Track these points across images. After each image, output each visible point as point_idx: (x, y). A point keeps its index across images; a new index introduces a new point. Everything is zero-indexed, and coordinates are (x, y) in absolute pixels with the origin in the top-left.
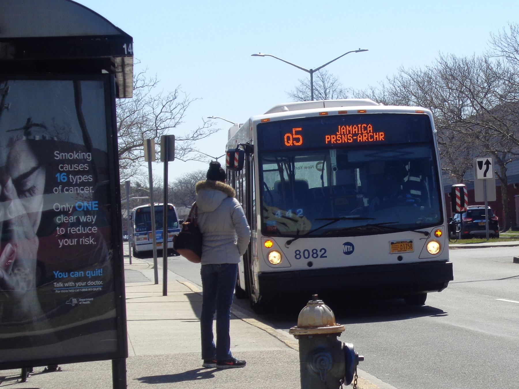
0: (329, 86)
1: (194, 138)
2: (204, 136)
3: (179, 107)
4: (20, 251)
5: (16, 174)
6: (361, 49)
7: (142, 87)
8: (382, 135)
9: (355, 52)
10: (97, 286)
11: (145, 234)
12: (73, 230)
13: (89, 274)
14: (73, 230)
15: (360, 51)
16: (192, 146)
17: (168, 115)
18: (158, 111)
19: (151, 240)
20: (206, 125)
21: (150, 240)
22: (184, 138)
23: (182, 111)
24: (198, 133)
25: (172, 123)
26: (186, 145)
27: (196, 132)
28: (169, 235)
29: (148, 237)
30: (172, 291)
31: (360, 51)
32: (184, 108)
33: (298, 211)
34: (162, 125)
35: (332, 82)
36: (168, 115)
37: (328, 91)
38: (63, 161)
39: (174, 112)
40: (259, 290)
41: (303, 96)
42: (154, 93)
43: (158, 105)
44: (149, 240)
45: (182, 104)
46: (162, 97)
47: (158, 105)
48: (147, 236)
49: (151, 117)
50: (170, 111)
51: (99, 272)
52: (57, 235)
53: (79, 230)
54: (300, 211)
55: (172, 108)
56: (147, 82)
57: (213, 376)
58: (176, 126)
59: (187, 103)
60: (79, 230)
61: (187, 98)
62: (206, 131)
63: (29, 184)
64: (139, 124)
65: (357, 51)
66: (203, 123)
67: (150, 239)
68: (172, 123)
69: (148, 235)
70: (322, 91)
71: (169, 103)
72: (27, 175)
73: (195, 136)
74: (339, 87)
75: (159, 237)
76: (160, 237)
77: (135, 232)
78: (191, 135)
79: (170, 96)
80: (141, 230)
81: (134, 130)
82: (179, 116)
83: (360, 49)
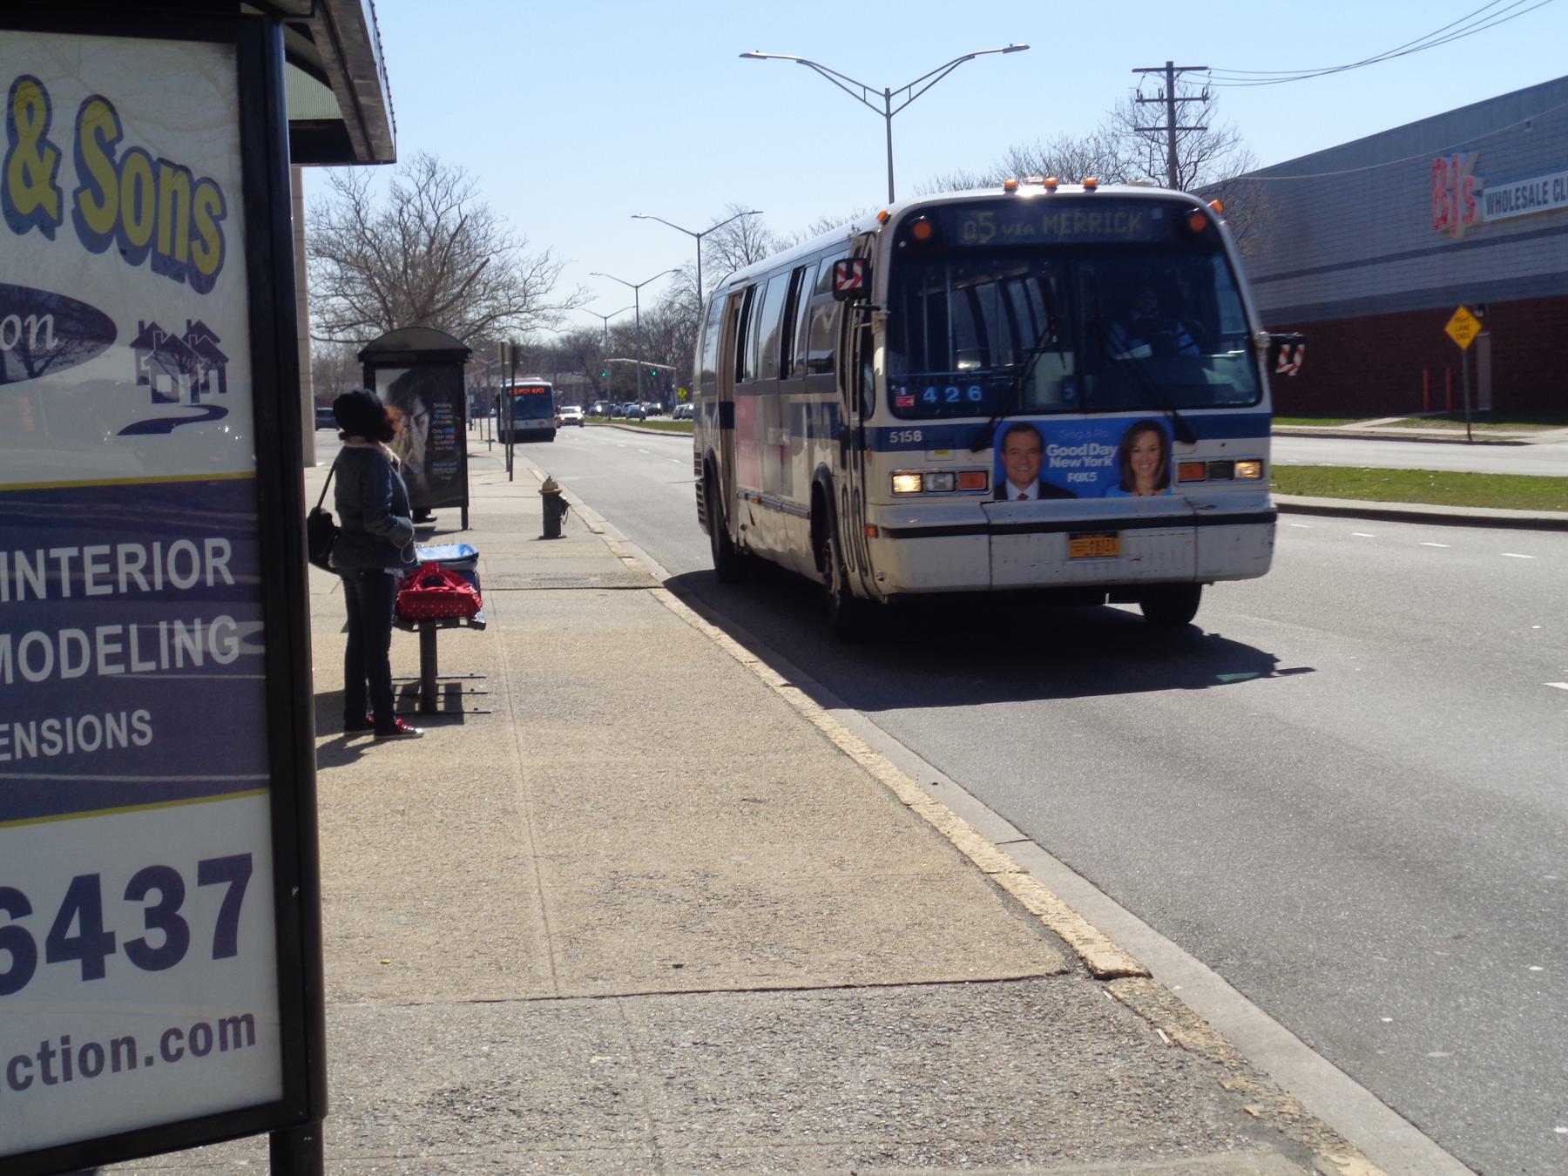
1: (567, 307)
3: (551, 271)
4: (416, 453)
5: (415, 415)
8: (218, 552)
10: (453, 470)
11: (976, 440)
12: (442, 443)
13: (451, 464)
14: (442, 443)
16: (567, 316)
17: (539, 280)
18: (526, 275)
19: (1023, 497)
21: (1013, 491)
22: (556, 306)
25: (543, 288)
29: (1000, 465)
30: (637, 592)
32: (557, 270)
34: (532, 291)
36: (539, 280)
38: (438, 408)
39: (545, 276)
42: (523, 254)
43: (527, 267)
44: (1001, 494)
47: (527, 267)
48: (986, 458)
49: (520, 280)
51: (455, 463)
52: (1000, 280)
53: (446, 442)
59: (560, 266)
60: (446, 442)
62: (581, 298)
63: (421, 420)
64: (507, 286)
67: (1015, 482)
68: (543, 288)
69: (1002, 449)
72: (420, 415)
77: (881, 417)
80: (930, 395)
81: (501, 293)
82: (551, 280)
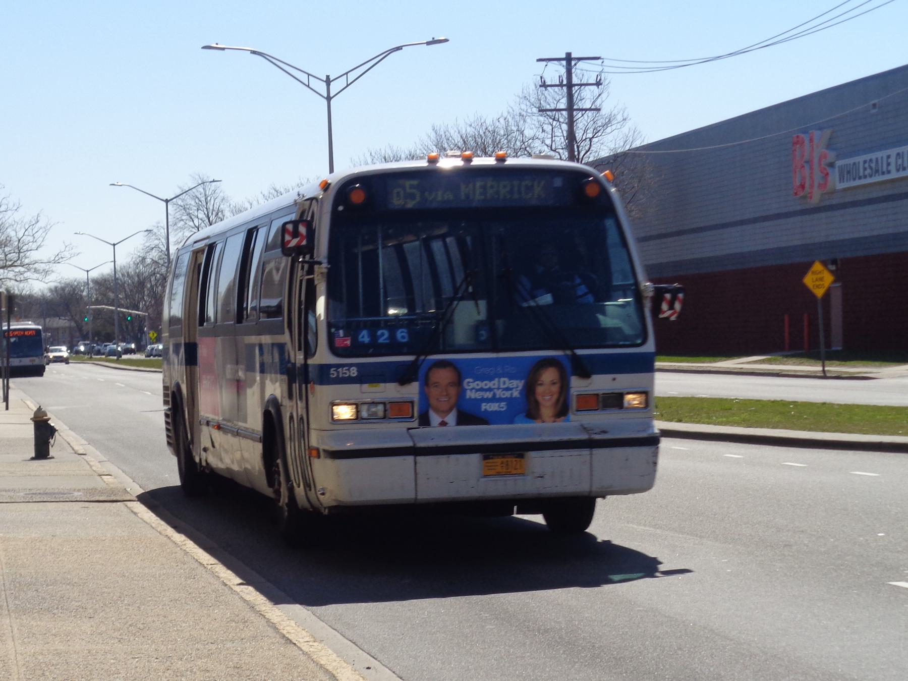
0: (210, 193)
2: (65, 259)
3: (41, 231)
6: (435, 39)
7: (5, 211)
9: (426, 44)
15: (434, 42)
16: (54, 269)
17: (31, 239)
18: (20, 235)
19: (443, 424)
20: (67, 249)
21: (435, 418)
22: (46, 261)
23: (44, 234)
24: (60, 256)
25: (34, 246)
26: (48, 267)
27: (58, 255)
28: (580, 397)
29: (424, 396)
31: (434, 42)
32: (46, 230)
33: (379, 333)
34: (25, 248)
35: (213, 189)
36: (31, 239)
37: (209, 199)
39: (35, 235)
40: (518, 518)
41: (182, 204)
42: (17, 216)
43: (21, 228)
44: (425, 421)
45: (44, 227)
46: (24, 221)
47: (21, 228)
48: (412, 391)
49: (15, 239)
50: (32, 235)
54: (383, 335)
55: (34, 232)
56: (10, 206)
57: (4, 401)
58: (38, 249)
59: (49, 227)
61: (50, 222)
62: (67, 254)
65: (428, 43)
66: (64, 247)
67: (437, 411)
68: (34, 246)
70: (203, 199)
71: (31, 227)
73: (57, 259)
74: (221, 194)
75: (500, 400)
76: (510, 401)
78: (53, 259)
79: (32, 220)
82: (41, 239)
83: (433, 38)
